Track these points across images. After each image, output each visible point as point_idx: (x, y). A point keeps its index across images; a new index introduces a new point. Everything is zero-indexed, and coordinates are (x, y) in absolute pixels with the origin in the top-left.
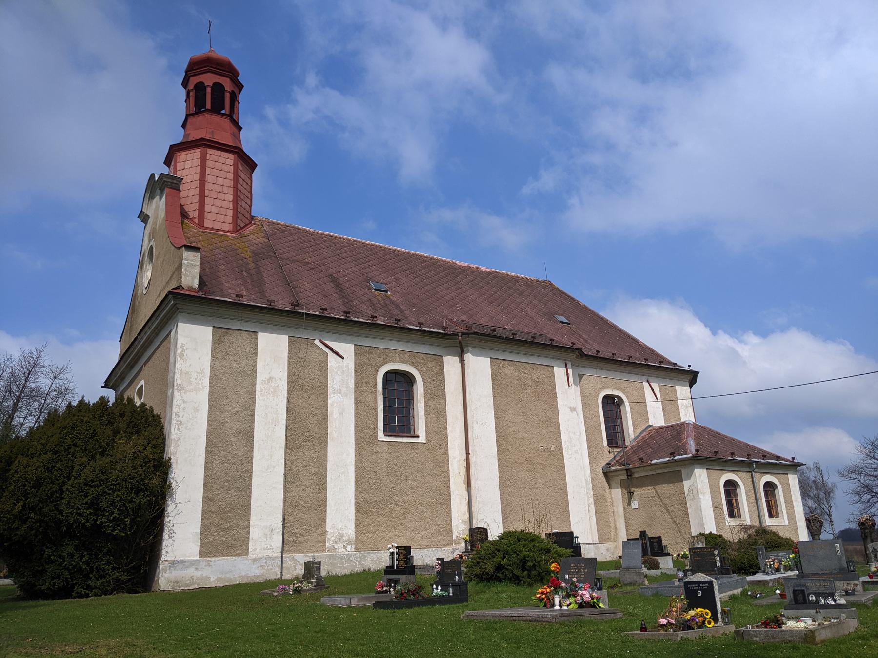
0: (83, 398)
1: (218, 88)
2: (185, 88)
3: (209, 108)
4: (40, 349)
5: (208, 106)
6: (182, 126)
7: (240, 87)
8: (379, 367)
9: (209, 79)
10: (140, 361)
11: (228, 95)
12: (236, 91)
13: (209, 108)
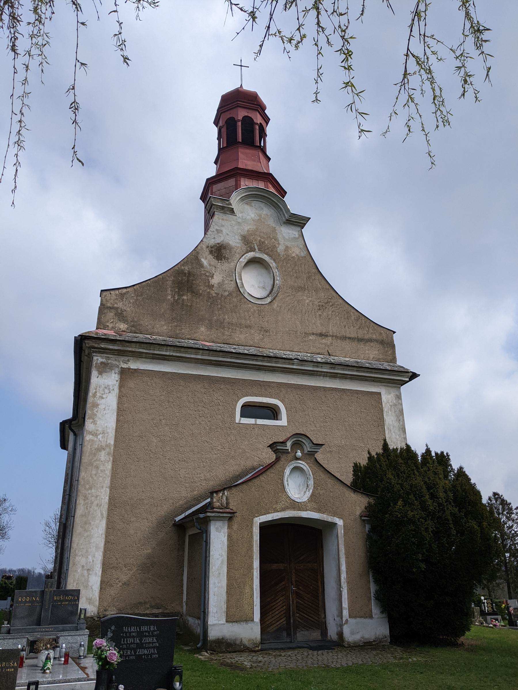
0: (369, 453)
1: (248, 122)
2: (217, 126)
3: (241, 141)
4: (346, 35)
5: (240, 139)
6: (201, 199)
7: (267, 120)
8: (282, 401)
9: (241, 114)
10: (254, 372)
11: (257, 127)
12: (264, 124)
13: (241, 141)
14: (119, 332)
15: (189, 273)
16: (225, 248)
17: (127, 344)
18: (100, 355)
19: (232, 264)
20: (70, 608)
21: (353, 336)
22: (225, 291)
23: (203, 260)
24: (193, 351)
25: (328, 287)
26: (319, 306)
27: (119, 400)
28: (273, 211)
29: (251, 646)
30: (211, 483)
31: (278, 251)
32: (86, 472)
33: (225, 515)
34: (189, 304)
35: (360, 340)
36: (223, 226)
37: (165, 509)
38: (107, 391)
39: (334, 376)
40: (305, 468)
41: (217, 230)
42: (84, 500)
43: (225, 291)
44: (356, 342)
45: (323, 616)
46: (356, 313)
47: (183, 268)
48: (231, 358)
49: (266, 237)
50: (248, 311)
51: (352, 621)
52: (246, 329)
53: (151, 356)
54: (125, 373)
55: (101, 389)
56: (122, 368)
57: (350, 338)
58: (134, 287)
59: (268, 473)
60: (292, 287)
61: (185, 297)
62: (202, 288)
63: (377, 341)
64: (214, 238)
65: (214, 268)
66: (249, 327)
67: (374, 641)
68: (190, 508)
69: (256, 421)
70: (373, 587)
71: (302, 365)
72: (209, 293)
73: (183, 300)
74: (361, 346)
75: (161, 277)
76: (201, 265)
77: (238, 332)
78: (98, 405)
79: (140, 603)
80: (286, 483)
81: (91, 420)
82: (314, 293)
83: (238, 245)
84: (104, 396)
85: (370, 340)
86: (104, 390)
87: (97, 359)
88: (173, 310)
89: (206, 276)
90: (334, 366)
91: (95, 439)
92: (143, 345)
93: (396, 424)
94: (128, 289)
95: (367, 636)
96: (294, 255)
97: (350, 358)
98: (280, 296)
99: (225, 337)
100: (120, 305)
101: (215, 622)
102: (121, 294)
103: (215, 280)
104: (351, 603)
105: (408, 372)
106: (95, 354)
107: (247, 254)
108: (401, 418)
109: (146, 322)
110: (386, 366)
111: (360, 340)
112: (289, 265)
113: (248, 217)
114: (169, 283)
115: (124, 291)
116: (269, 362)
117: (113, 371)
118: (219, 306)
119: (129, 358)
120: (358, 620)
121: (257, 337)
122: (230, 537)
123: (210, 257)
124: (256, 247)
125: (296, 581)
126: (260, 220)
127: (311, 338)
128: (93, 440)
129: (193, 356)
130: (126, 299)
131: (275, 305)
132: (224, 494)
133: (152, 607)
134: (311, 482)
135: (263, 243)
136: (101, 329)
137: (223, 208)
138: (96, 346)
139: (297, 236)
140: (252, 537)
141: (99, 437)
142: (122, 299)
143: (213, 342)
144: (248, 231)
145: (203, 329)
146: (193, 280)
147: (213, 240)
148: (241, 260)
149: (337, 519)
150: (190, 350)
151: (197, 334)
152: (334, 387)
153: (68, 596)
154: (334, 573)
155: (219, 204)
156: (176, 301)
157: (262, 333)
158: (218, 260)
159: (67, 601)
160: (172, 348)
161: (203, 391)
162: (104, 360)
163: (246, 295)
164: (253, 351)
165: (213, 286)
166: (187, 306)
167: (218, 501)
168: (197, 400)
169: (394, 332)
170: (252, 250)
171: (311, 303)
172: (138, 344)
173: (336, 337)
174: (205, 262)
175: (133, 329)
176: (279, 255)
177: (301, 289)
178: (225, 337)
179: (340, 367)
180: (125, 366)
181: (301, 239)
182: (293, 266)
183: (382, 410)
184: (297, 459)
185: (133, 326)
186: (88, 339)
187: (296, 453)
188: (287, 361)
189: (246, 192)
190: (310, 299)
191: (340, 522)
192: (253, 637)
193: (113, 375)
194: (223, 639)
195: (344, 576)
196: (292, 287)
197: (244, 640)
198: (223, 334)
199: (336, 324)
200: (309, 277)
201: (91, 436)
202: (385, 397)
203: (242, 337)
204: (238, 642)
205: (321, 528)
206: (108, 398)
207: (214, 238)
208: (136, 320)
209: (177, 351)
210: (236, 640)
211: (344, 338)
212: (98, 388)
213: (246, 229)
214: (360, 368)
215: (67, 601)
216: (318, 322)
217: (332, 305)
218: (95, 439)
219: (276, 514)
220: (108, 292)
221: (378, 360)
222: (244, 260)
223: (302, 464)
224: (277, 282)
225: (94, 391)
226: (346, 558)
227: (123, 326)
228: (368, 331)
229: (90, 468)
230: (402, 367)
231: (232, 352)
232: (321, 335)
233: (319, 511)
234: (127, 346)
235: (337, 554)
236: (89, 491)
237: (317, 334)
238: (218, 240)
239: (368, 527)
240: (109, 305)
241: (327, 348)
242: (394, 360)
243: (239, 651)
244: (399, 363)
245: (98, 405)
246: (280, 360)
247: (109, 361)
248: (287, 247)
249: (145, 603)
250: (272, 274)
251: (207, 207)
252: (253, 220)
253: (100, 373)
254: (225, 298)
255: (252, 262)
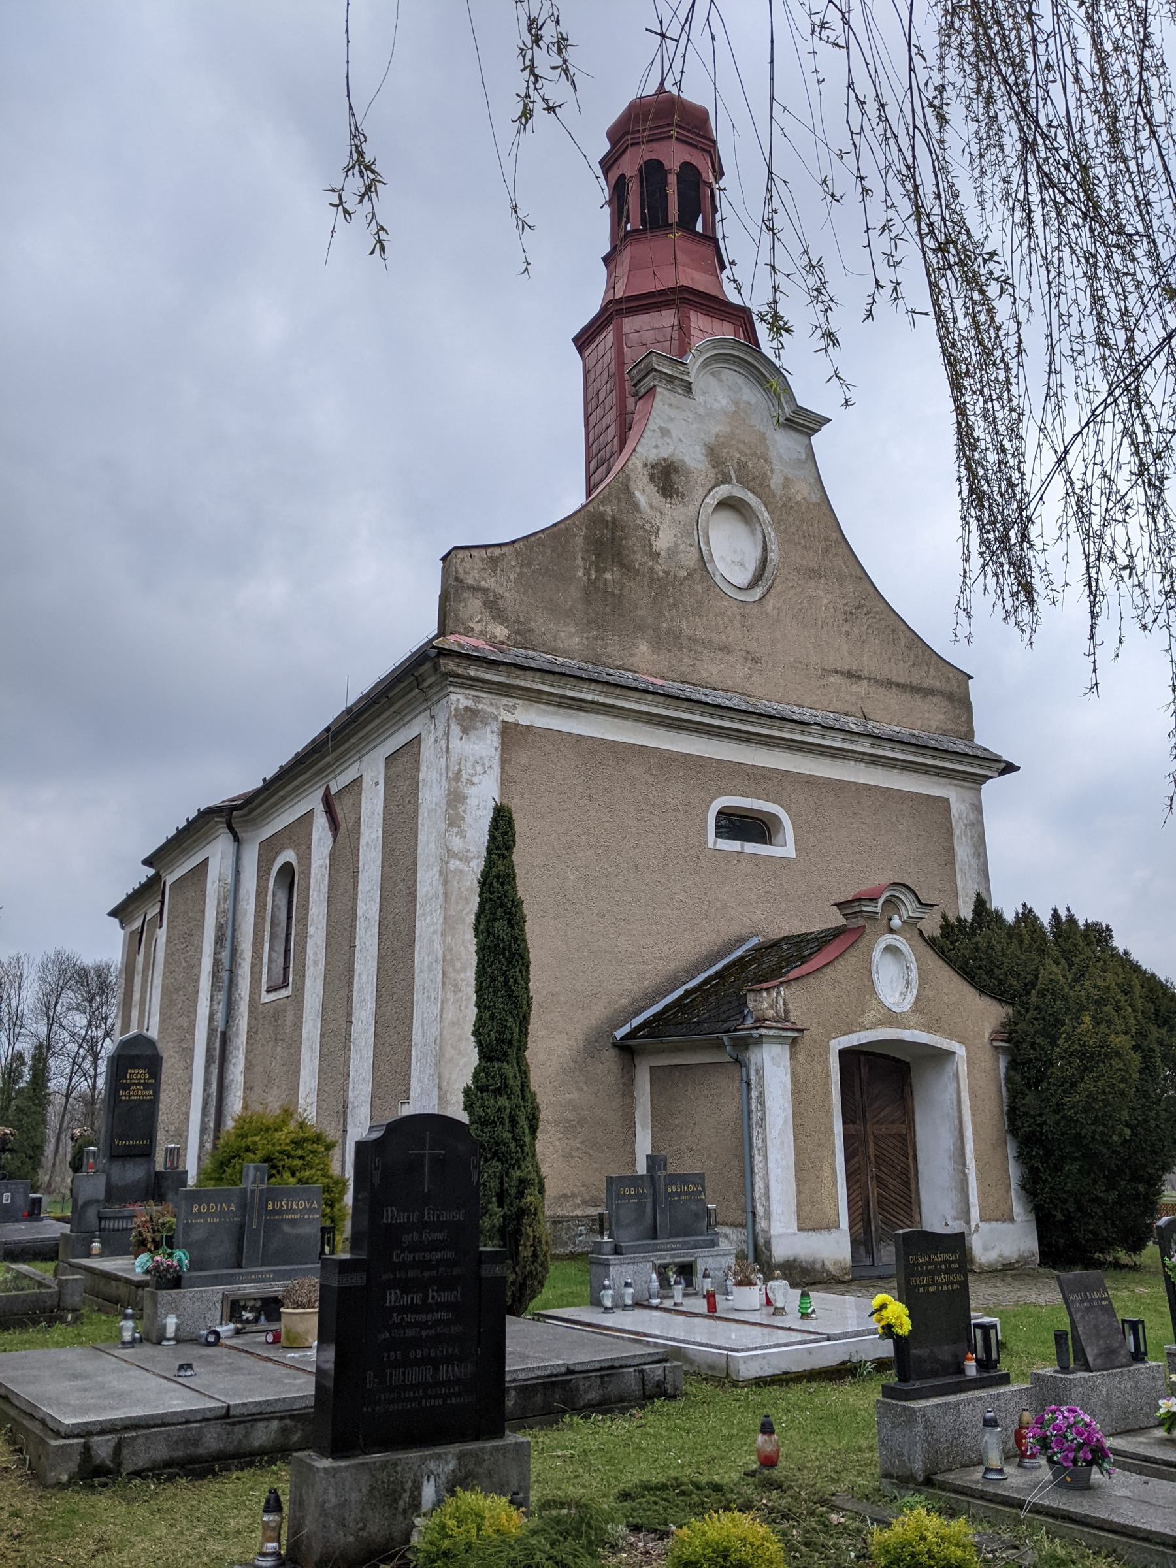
8: (787, 809)
14: (498, 645)
15: (614, 521)
16: (677, 471)
17: (519, 672)
18: (462, 691)
19: (692, 509)
20: (693, 1207)
21: (902, 680)
22: (681, 567)
23: (638, 494)
24: (637, 695)
25: (859, 573)
26: (845, 612)
27: (502, 789)
28: (759, 396)
29: (837, 1273)
30: (673, 965)
31: (772, 487)
32: (453, 936)
33: (785, 1034)
34: (617, 592)
35: (914, 690)
36: (671, 420)
37: (598, 1013)
38: (479, 769)
39: (874, 761)
40: (903, 948)
41: (661, 428)
42: (455, 993)
43: (681, 567)
44: (908, 695)
45: (918, 1219)
46: (909, 634)
47: (601, 508)
48: (703, 714)
49: (748, 452)
50: (723, 615)
51: (984, 1226)
52: (720, 655)
53: (558, 700)
54: (511, 735)
55: (469, 765)
56: (503, 721)
57: (898, 685)
58: (516, 545)
59: (847, 956)
60: (798, 569)
61: (608, 576)
62: (638, 556)
63: (942, 693)
64: (656, 447)
65: (658, 514)
66: (725, 649)
67: (1017, 1262)
68: (637, 1013)
69: (742, 847)
70: (1014, 1171)
71: (823, 736)
72: (652, 570)
73: (606, 580)
74: (917, 702)
75: (563, 525)
76: (636, 507)
77: (707, 660)
78: (465, 798)
79: (565, 1196)
80: (875, 976)
81: (456, 830)
82: (836, 586)
83: (701, 467)
84: (475, 780)
85: (931, 692)
86: (474, 767)
87: (458, 700)
88: (588, 602)
89: (645, 530)
90: (877, 742)
91: (466, 869)
92: (547, 676)
93: (974, 862)
94: (505, 550)
95: (1007, 1253)
96: (799, 498)
97: (898, 725)
98: (778, 588)
99: (683, 669)
100: (490, 583)
101: (782, 1231)
102: (491, 558)
103: (662, 543)
104: (983, 1196)
105: (999, 761)
106: (452, 689)
107: (717, 489)
108: (981, 850)
109: (541, 624)
110: (960, 746)
111: (914, 690)
112: (791, 519)
113: (716, 406)
114: (580, 541)
115: (497, 552)
116: (767, 727)
117: (488, 728)
118: (671, 600)
119: (516, 701)
120: (994, 1224)
121: (741, 671)
122: (794, 1075)
123: (651, 488)
124: (733, 476)
125: (876, 1156)
126: (738, 415)
127: (832, 679)
128: (461, 871)
129: (634, 706)
130: (502, 570)
131: (770, 603)
132: (779, 993)
133: (586, 1203)
134: (914, 976)
135: (745, 465)
136: (459, 633)
137: (671, 379)
138: (460, 671)
139: (804, 456)
140: (828, 1076)
141: (471, 864)
142: (494, 571)
143: (663, 677)
144: (717, 436)
145: (644, 648)
146: (621, 539)
147: (655, 451)
148: (707, 500)
149: (957, 1045)
150: (630, 693)
151: (635, 659)
152: (872, 783)
153: (687, 1183)
154: (947, 1141)
155: (666, 371)
156: (592, 583)
157: (748, 664)
158: (665, 496)
159: (686, 1193)
160: (599, 687)
161: (650, 779)
162: (470, 703)
163: (718, 579)
164: (735, 702)
165: (658, 554)
166: (613, 595)
167: (771, 1006)
168: (640, 798)
169: (971, 677)
170: (725, 480)
171: (831, 606)
172: (538, 674)
173: (876, 681)
174: (641, 499)
175: (519, 638)
176: (774, 495)
177: (813, 573)
178: (683, 669)
179: (890, 745)
180: (509, 718)
181: (810, 462)
182: (799, 523)
183: (951, 835)
184: (891, 931)
185: (518, 633)
186: (445, 655)
187: (890, 919)
188: (800, 727)
189: (715, 348)
190: (829, 596)
191: (960, 1050)
192: (841, 1258)
193: (489, 736)
194: (795, 1260)
195: (970, 1147)
196: (798, 569)
197: (826, 1262)
198: (681, 662)
199: (875, 653)
200: (826, 550)
201: (458, 863)
202: (958, 807)
203: (714, 670)
204: (818, 1266)
205: (908, 1060)
206: (483, 783)
207: (656, 447)
208: (522, 618)
209: (606, 694)
210: (814, 1262)
211: (888, 684)
212: (463, 762)
213: (713, 431)
214: (921, 747)
215: (686, 1193)
216: (845, 647)
217: (868, 613)
218: (466, 869)
219: (863, 1033)
220: (467, 553)
221: (944, 733)
222: (712, 501)
223: (898, 941)
224: (771, 555)
225: (457, 767)
226: (973, 1115)
227: (500, 632)
228: (927, 672)
229: (460, 927)
230: (986, 750)
231: (706, 703)
232: (850, 675)
233: (930, 1029)
234: (518, 677)
235: (955, 1108)
236: (462, 976)
237: (842, 673)
238: (665, 453)
239: (1002, 1065)
240: (470, 581)
241: (860, 704)
242: (969, 735)
243: (820, 1283)
244: (978, 741)
245: (465, 798)
246: (788, 725)
247: (480, 706)
248: (786, 479)
249: (574, 1195)
250: (760, 536)
251: (635, 371)
252: (725, 413)
253: (465, 730)
254: (681, 584)
255: (728, 504)
